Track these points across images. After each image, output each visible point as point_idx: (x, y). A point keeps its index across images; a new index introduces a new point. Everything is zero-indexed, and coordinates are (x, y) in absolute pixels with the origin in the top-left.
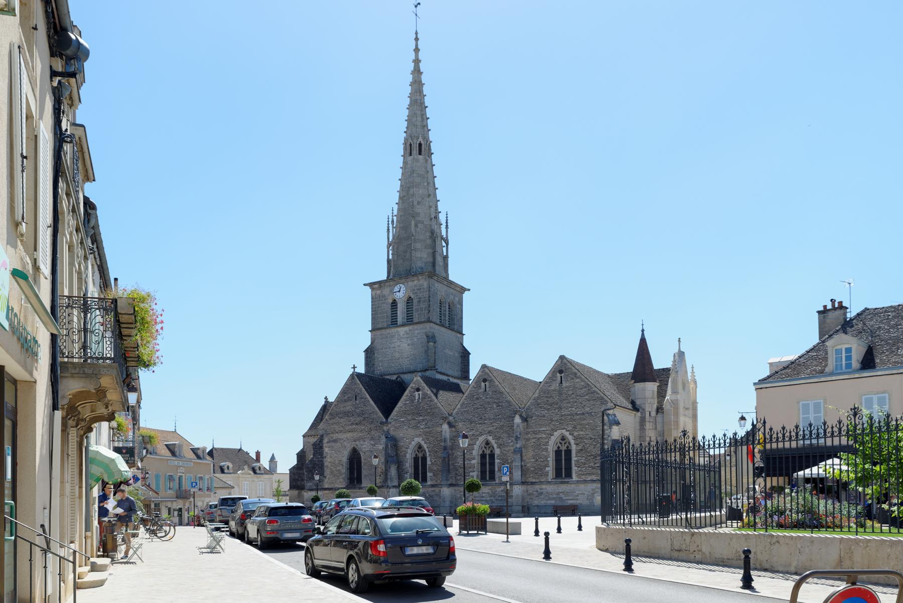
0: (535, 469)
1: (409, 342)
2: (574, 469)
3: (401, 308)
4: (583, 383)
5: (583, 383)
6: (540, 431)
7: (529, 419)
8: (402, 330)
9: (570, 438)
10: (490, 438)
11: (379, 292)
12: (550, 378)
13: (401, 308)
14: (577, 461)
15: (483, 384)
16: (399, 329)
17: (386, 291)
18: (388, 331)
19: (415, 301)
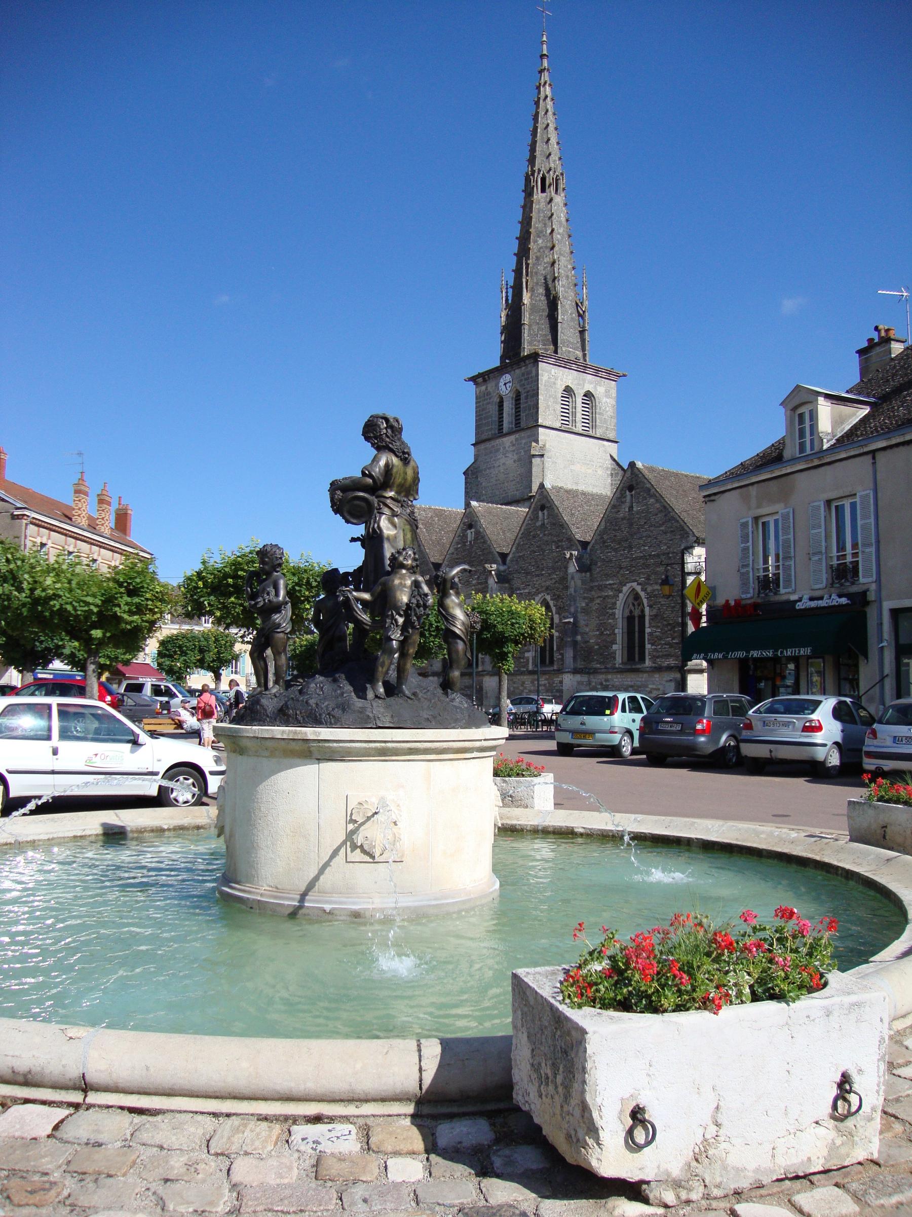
0: (600, 648)
1: (516, 457)
2: (648, 646)
3: (508, 407)
4: (658, 505)
5: (658, 505)
6: (606, 586)
7: (593, 567)
8: (507, 441)
9: (642, 594)
10: (548, 598)
11: (483, 388)
12: (618, 498)
13: (508, 407)
14: (650, 634)
15: (540, 513)
16: (505, 439)
17: (491, 386)
18: (493, 443)
19: (523, 397)
